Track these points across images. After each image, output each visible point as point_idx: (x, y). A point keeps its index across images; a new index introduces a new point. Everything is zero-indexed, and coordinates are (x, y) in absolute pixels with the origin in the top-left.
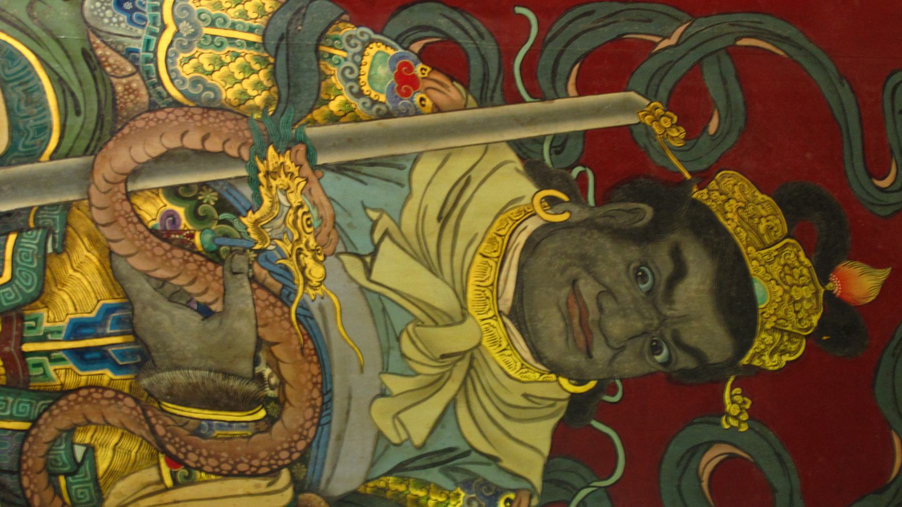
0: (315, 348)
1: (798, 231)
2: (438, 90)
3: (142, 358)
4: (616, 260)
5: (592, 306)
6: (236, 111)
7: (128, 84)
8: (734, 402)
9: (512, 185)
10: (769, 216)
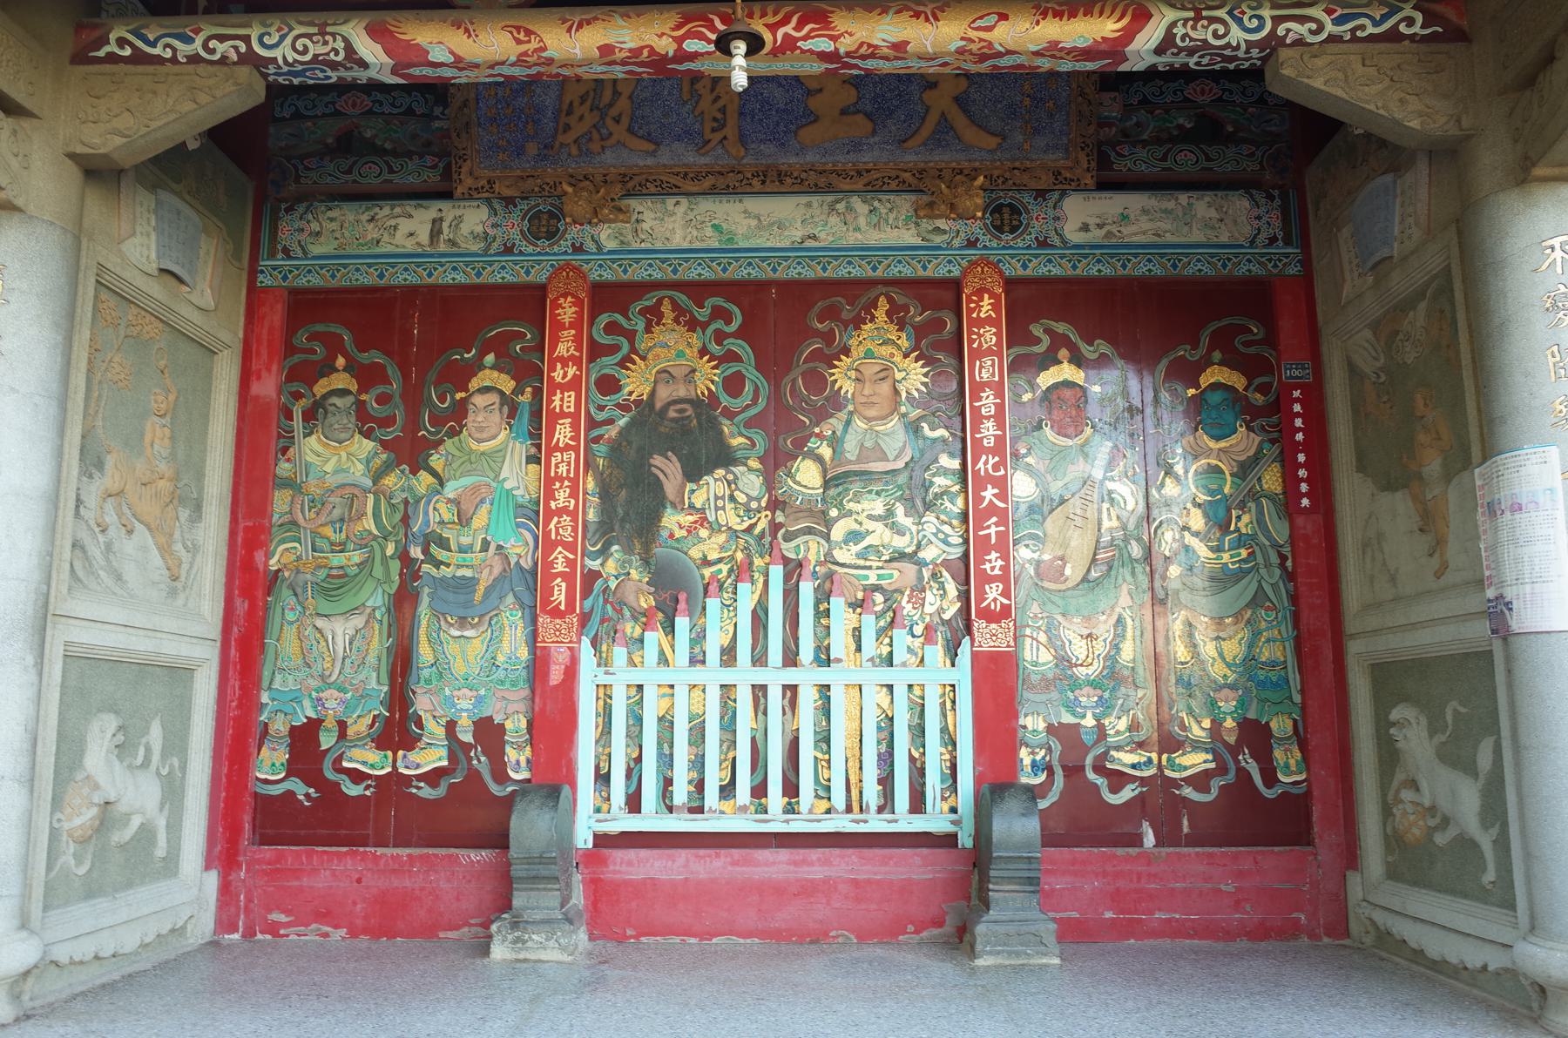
0: (343, 486)
1: (328, 375)
2: (291, 452)
3: (342, 520)
4: (331, 419)
5: (1032, 929)
6: (293, 497)
7: (286, 518)
8: (363, 397)
9: (313, 439)
10: (323, 381)
